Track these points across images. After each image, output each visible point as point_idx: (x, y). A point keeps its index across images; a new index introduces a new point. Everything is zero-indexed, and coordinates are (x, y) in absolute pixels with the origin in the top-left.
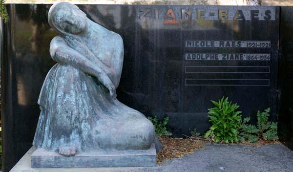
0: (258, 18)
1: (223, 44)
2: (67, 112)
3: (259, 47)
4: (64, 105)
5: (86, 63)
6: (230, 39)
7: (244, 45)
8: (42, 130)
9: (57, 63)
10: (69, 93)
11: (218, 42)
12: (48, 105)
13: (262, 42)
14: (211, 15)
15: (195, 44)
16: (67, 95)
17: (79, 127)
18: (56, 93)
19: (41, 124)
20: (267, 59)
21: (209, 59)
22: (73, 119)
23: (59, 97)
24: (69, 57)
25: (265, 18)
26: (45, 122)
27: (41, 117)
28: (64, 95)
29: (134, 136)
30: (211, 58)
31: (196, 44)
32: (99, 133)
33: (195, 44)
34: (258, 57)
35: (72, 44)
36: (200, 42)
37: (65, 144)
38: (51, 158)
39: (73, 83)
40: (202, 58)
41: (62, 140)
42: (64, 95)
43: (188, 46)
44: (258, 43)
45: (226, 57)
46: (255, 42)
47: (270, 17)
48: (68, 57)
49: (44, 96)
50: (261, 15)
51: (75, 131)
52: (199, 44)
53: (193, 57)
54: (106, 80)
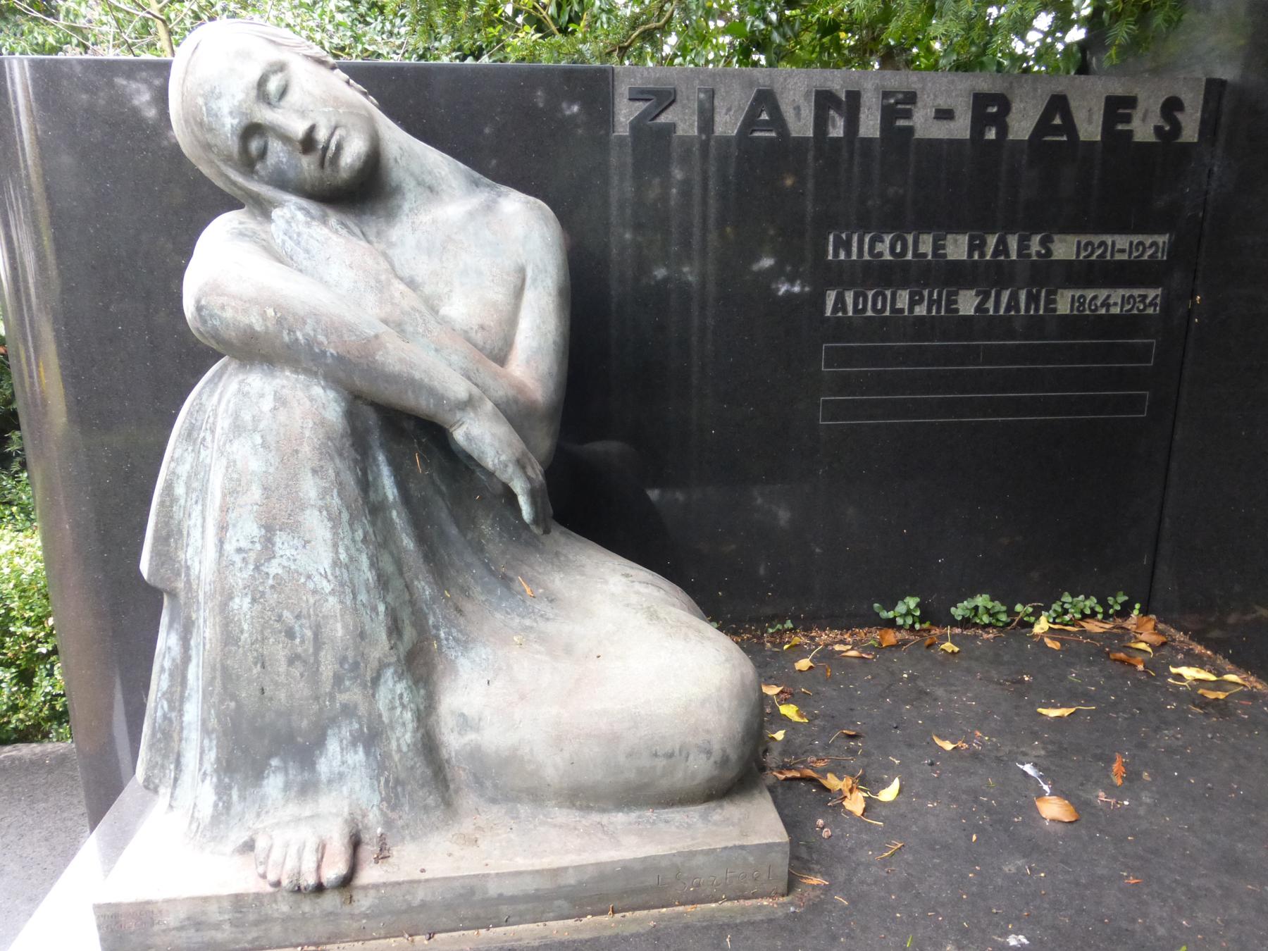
0: (1130, 133)
1: (982, 247)
2: (290, 634)
3: (1125, 257)
4: (272, 598)
5: (379, 357)
6: (1009, 228)
7: (1065, 248)
8: (171, 708)
9: (220, 356)
10: (293, 528)
11: (964, 240)
12: (188, 582)
13: (1136, 239)
14: (945, 114)
15: (866, 247)
16: (280, 538)
17: (362, 710)
18: (223, 528)
19: (165, 676)
20: (1150, 311)
21: (921, 310)
22: (328, 669)
23: (239, 550)
24: (280, 321)
25: (1158, 130)
26: (179, 674)
27: (167, 641)
28: (268, 542)
29: (668, 749)
30: (929, 310)
31: (872, 247)
32: (477, 729)
33: (866, 247)
34: (1115, 300)
35: (307, 251)
36: (888, 239)
37: (292, 809)
38: (213, 908)
39: (314, 471)
40: (893, 310)
41: (273, 784)
42: (268, 542)
43: (836, 254)
44: (1122, 241)
45: (990, 305)
46: (1109, 239)
47: (1177, 128)
48: (271, 325)
49: (170, 536)
50: (1144, 120)
51: (345, 732)
52: (884, 247)
53: (856, 304)
54: (484, 437)
